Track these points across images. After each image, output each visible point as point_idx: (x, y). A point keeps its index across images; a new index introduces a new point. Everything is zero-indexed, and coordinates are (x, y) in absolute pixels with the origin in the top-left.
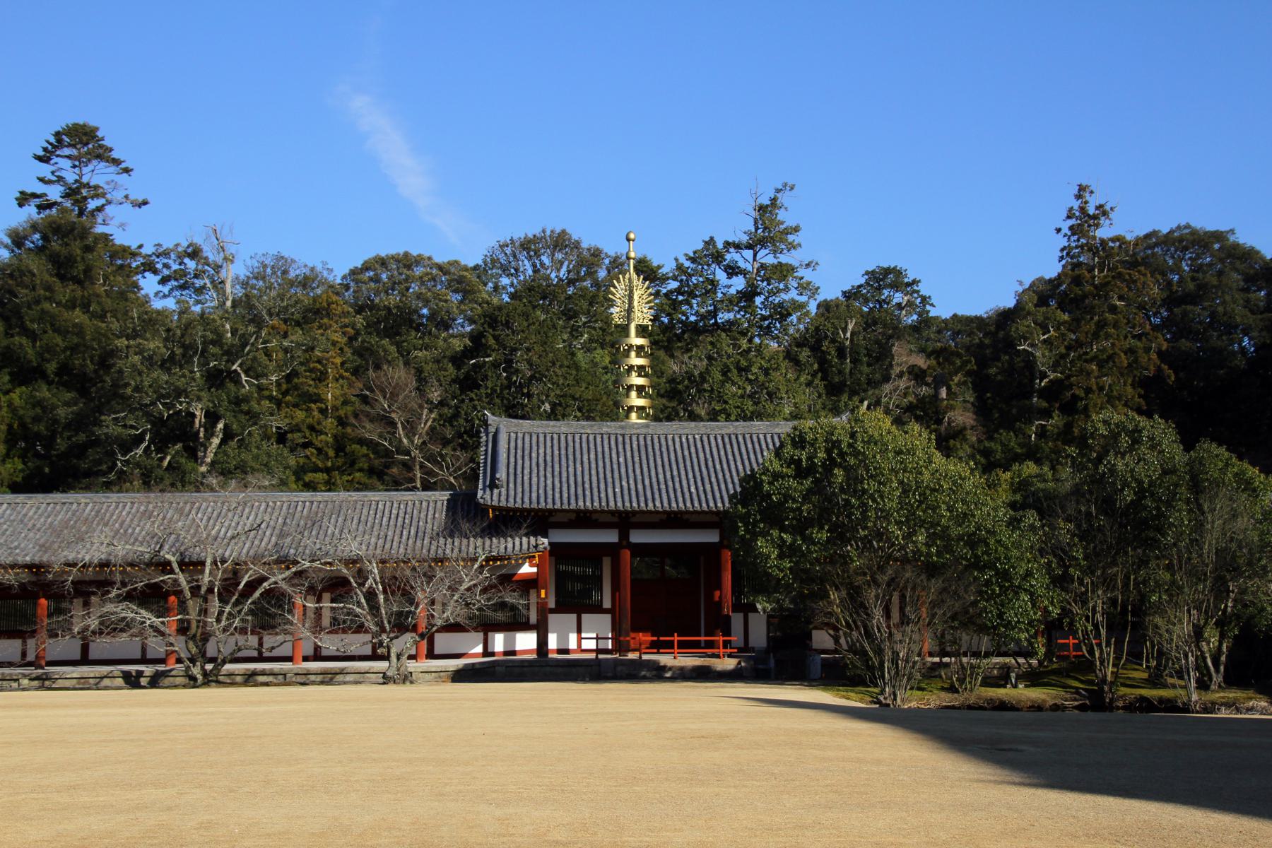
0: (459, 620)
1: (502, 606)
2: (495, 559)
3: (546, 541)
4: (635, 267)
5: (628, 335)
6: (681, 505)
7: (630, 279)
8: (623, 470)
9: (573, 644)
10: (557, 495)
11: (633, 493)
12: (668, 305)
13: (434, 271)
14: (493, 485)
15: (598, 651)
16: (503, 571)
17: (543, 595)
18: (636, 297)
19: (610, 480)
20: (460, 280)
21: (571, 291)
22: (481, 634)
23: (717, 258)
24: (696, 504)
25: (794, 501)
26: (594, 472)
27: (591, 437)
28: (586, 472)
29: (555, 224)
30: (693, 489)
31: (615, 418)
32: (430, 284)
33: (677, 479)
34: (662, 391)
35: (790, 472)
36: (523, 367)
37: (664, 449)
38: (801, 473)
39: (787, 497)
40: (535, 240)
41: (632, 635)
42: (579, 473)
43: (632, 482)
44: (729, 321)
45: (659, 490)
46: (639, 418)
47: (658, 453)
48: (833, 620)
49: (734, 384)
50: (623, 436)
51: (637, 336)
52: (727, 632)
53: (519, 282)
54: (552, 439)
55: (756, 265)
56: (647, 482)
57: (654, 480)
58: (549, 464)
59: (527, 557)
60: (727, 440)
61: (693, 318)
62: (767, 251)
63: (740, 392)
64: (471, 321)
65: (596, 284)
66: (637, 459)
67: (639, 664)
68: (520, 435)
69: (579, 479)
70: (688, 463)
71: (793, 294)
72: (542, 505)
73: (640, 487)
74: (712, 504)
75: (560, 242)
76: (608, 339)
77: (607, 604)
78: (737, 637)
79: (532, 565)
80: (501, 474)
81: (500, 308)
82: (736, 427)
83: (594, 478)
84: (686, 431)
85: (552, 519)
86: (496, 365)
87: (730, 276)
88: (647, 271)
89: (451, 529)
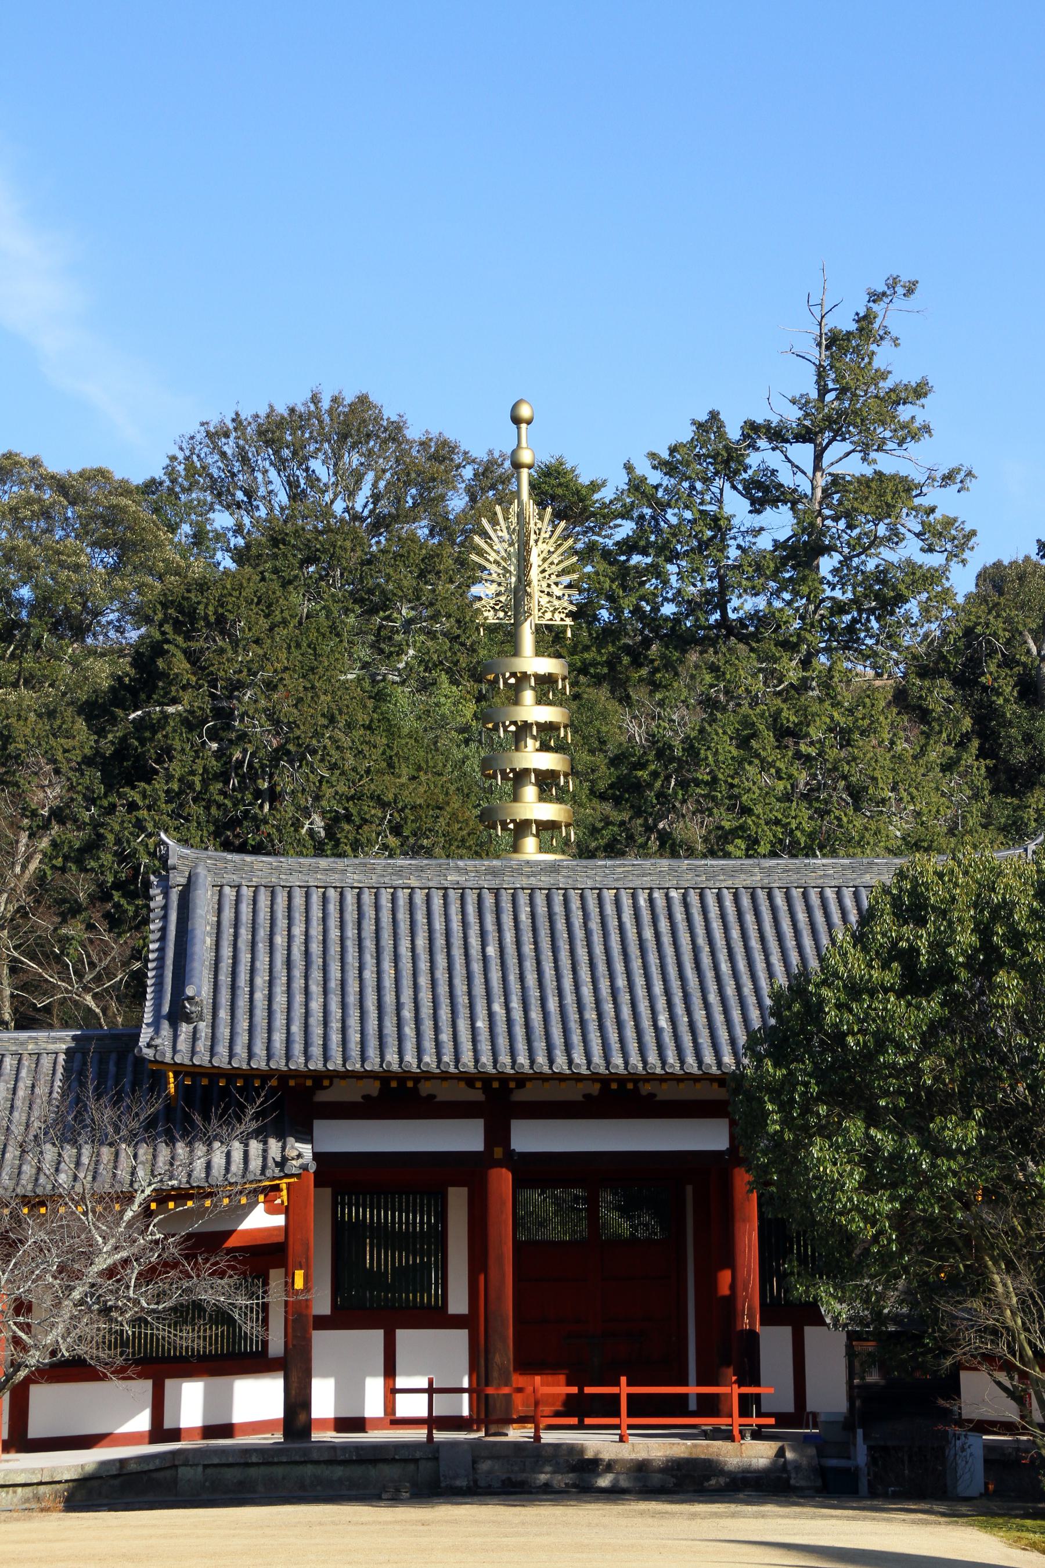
0: (81, 1350)
1: (189, 1312)
2: (181, 1195)
3: (306, 1150)
4: (533, 486)
5: (516, 653)
6: (635, 1059)
7: (520, 515)
8: (495, 975)
9: (373, 1407)
10: (335, 1038)
11: (519, 1031)
12: (609, 576)
13: (47, 495)
14: (178, 1014)
15: (432, 1422)
16: (196, 1226)
17: (299, 1284)
18: (535, 559)
19: (462, 1000)
20: (111, 514)
21: (377, 543)
22: (147, 1385)
23: (727, 462)
24: (671, 1058)
25: (903, 1050)
26: (424, 981)
27: (419, 897)
28: (407, 982)
29: (341, 382)
30: (663, 1022)
31: (481, 850)
32: (38, 526)
33: (625, 998)
34: (602, 786)
35: (889, 978)
36: (259, 728)
37: (595, 925)
38: (916, 983)
39: (883, 1040)
40: (296, 420)
41: (518, 1380)
42: (388, 982)
43: (515, 1004)
44: (755, 616)
45: (582, 1023)
46: (541, 849)
47: (579, 934)
48: (1003, 1349)
49: (765, 766)
50: (496, 892)
51: (538, 653)
52: (750, 1375)
53: (256, 522)
54: (325, 899)
55: (821, 481)
56: (552, 1004)
57: (570, 999)
58: (317, 961)
59: (257, 1185)
60: (746, 901)
61: (668, 609)
62: (847, 446)
63: (780, 785)
64: (142, 617)
65: (442, 527)
66: (528, 949)
67: (533, 1454)
68: (247, 893)
69: (389, 998)
70: (653, 959)
71: (911, 550)
72: (298, 1062)
73: (536, 1015)
74: (709, 1058)
75: (355, 425)
76: (464, 661)
77: (458, 1304)
78: (775, 1388)
79: (271, 1210)
80: (199, 987)
81: (202, 586)
82: (769, 872)
83: (425, 996)
84: (647, 882)
85: (322, 1097)
86: (191, 723)
87: (758, 506)
88: (561, 495)
89: (70, 1125)
